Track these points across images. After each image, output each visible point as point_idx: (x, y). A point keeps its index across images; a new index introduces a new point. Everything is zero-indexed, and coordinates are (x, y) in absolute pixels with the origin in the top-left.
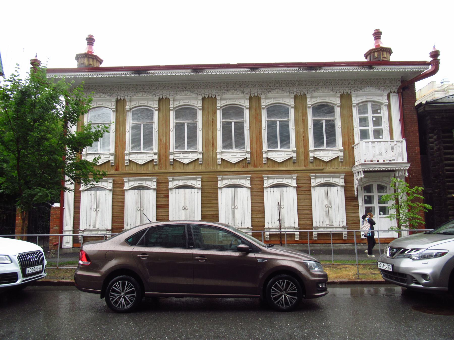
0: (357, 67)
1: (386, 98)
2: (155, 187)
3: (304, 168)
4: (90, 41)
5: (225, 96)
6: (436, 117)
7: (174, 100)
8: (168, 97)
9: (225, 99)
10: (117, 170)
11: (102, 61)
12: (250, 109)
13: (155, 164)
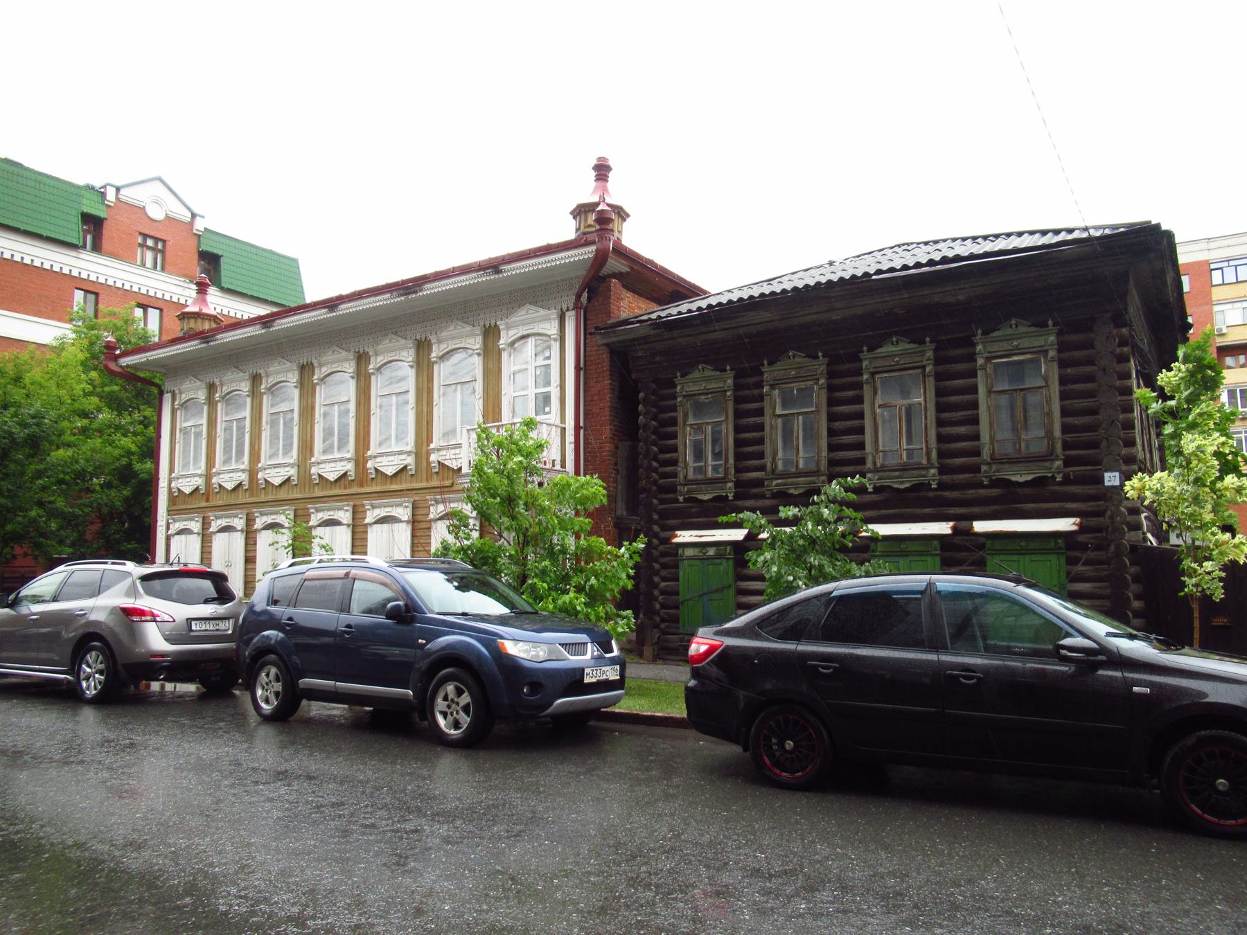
0: (475, 275)
1: (556, 324)
3: (424, 484)
4: (602, 170)
5: (514, 319)
6: (640, 354)
7: (267, 376)
8: (367, 350)
9: (326, 364)
10: (207, 500)
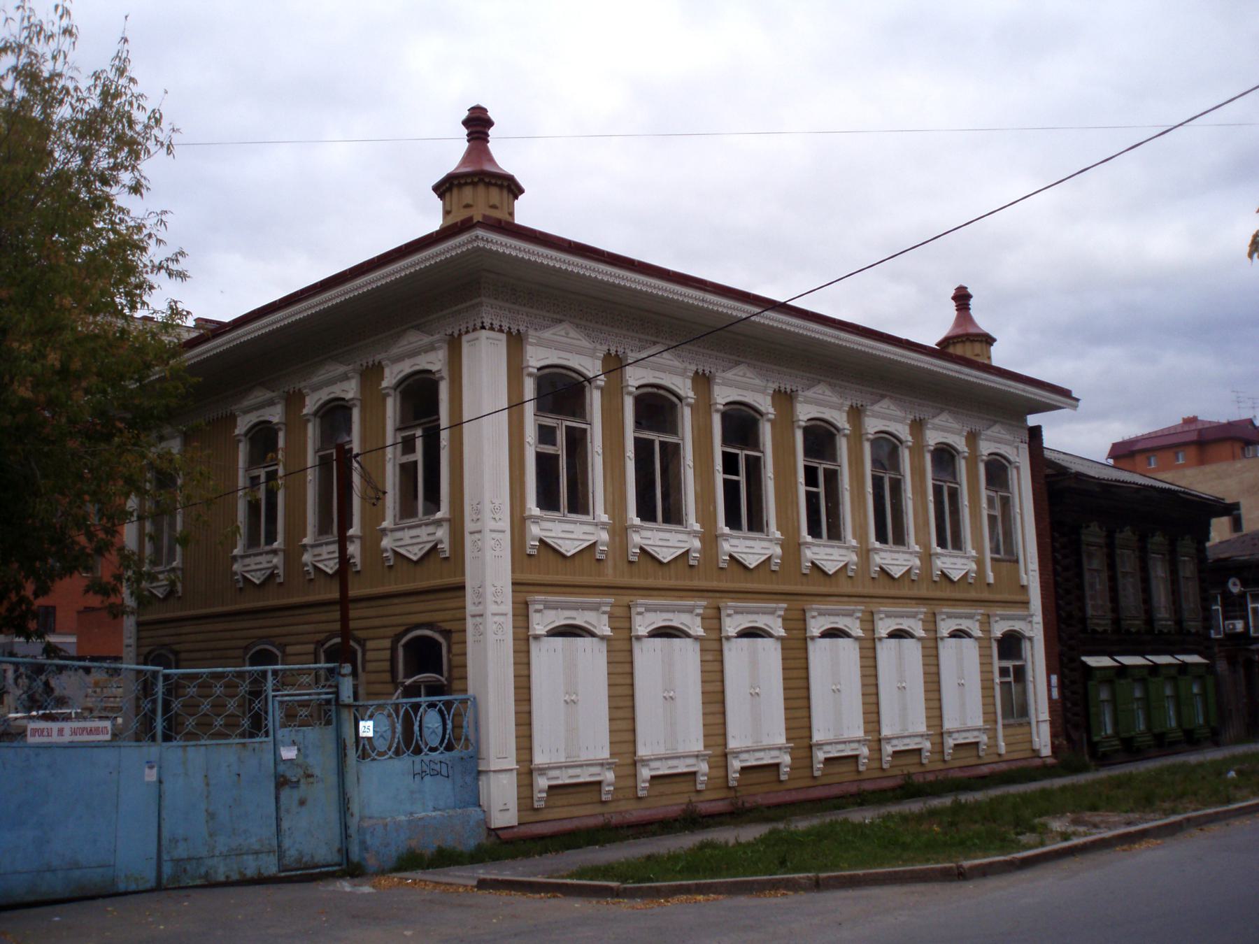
2: (782, 633)
4: (478, 123)
12: (773, 422)
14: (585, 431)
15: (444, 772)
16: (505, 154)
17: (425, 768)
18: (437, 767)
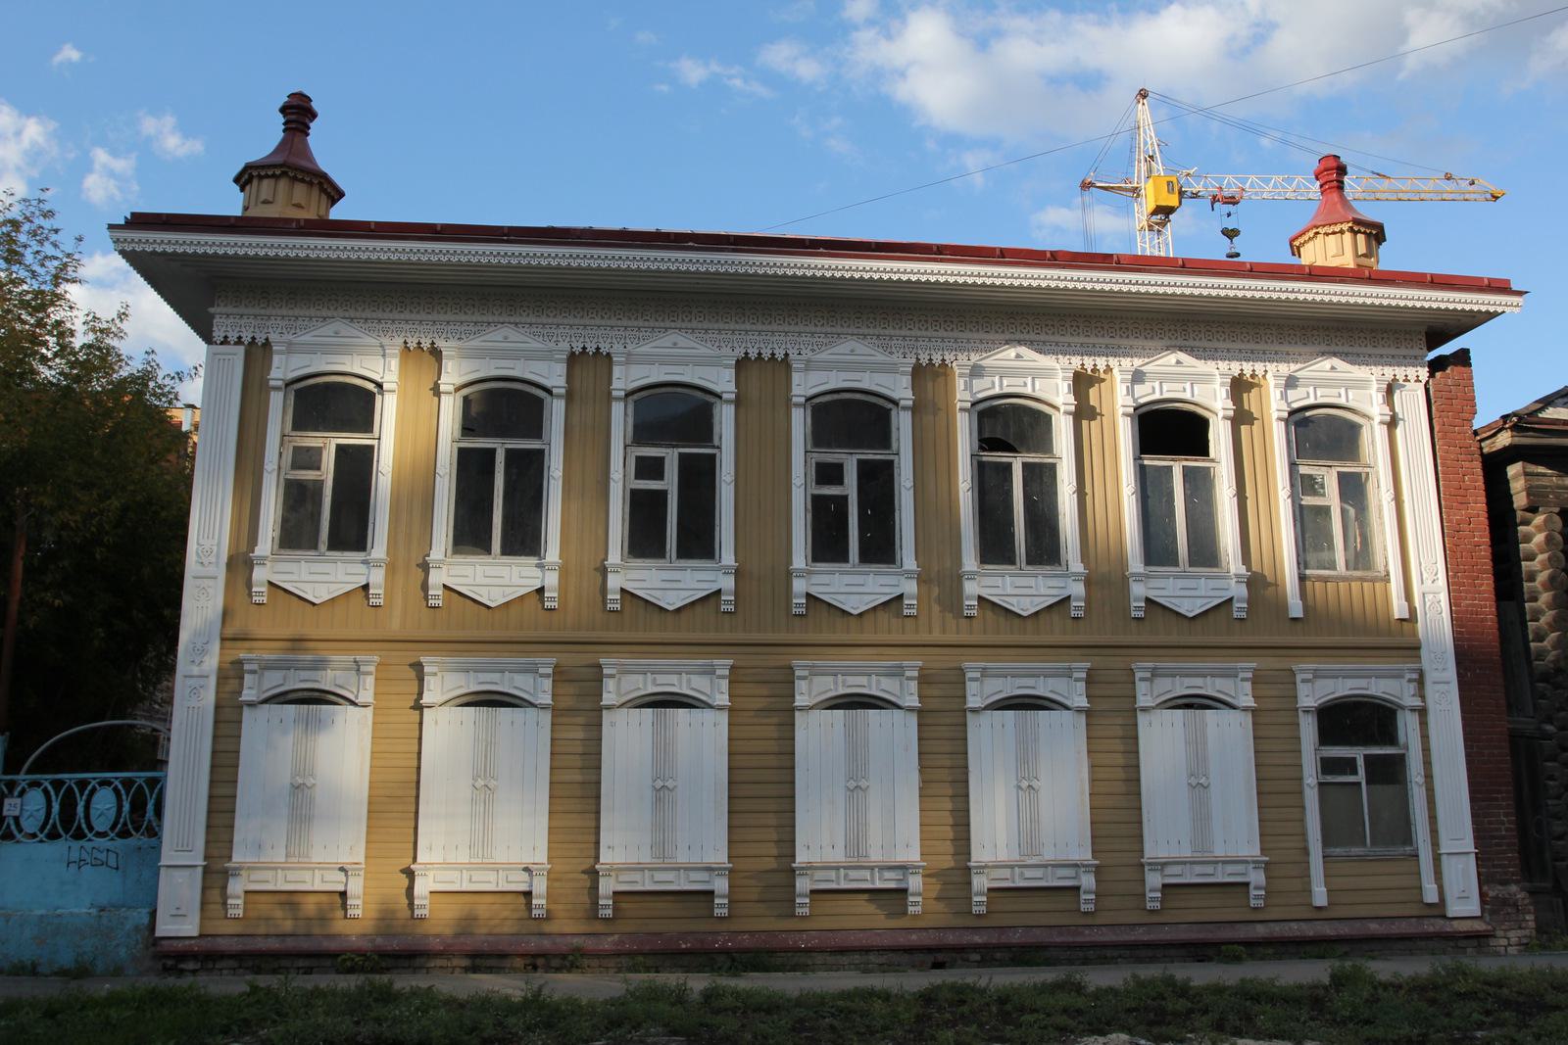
2: (1250, 702)
11: (341, 195)
13: (906, 612)
14: (714, 456)
15: (112, 862)
16: (324, 147)
17: (84, 855)
18: (103, 856)
